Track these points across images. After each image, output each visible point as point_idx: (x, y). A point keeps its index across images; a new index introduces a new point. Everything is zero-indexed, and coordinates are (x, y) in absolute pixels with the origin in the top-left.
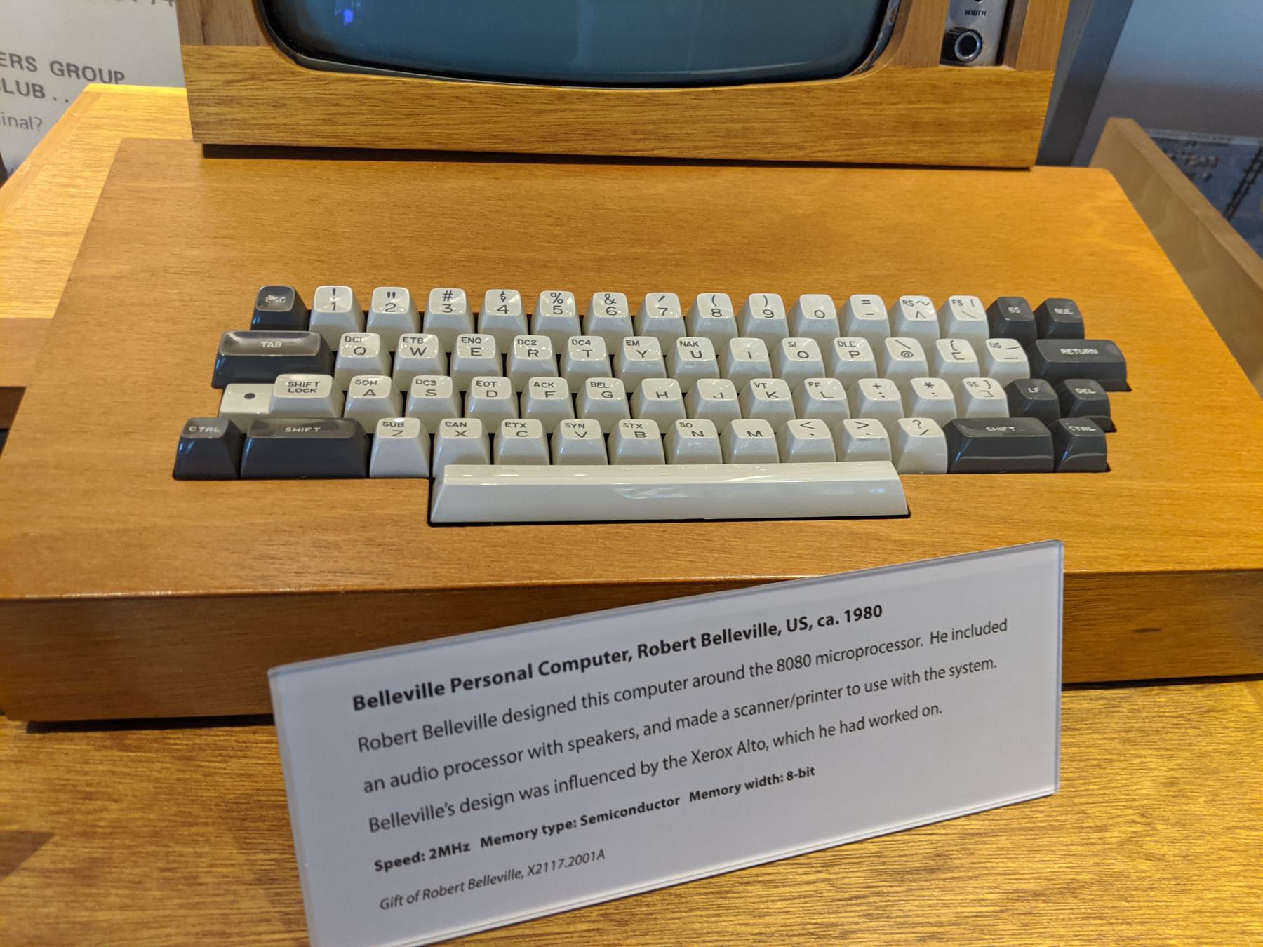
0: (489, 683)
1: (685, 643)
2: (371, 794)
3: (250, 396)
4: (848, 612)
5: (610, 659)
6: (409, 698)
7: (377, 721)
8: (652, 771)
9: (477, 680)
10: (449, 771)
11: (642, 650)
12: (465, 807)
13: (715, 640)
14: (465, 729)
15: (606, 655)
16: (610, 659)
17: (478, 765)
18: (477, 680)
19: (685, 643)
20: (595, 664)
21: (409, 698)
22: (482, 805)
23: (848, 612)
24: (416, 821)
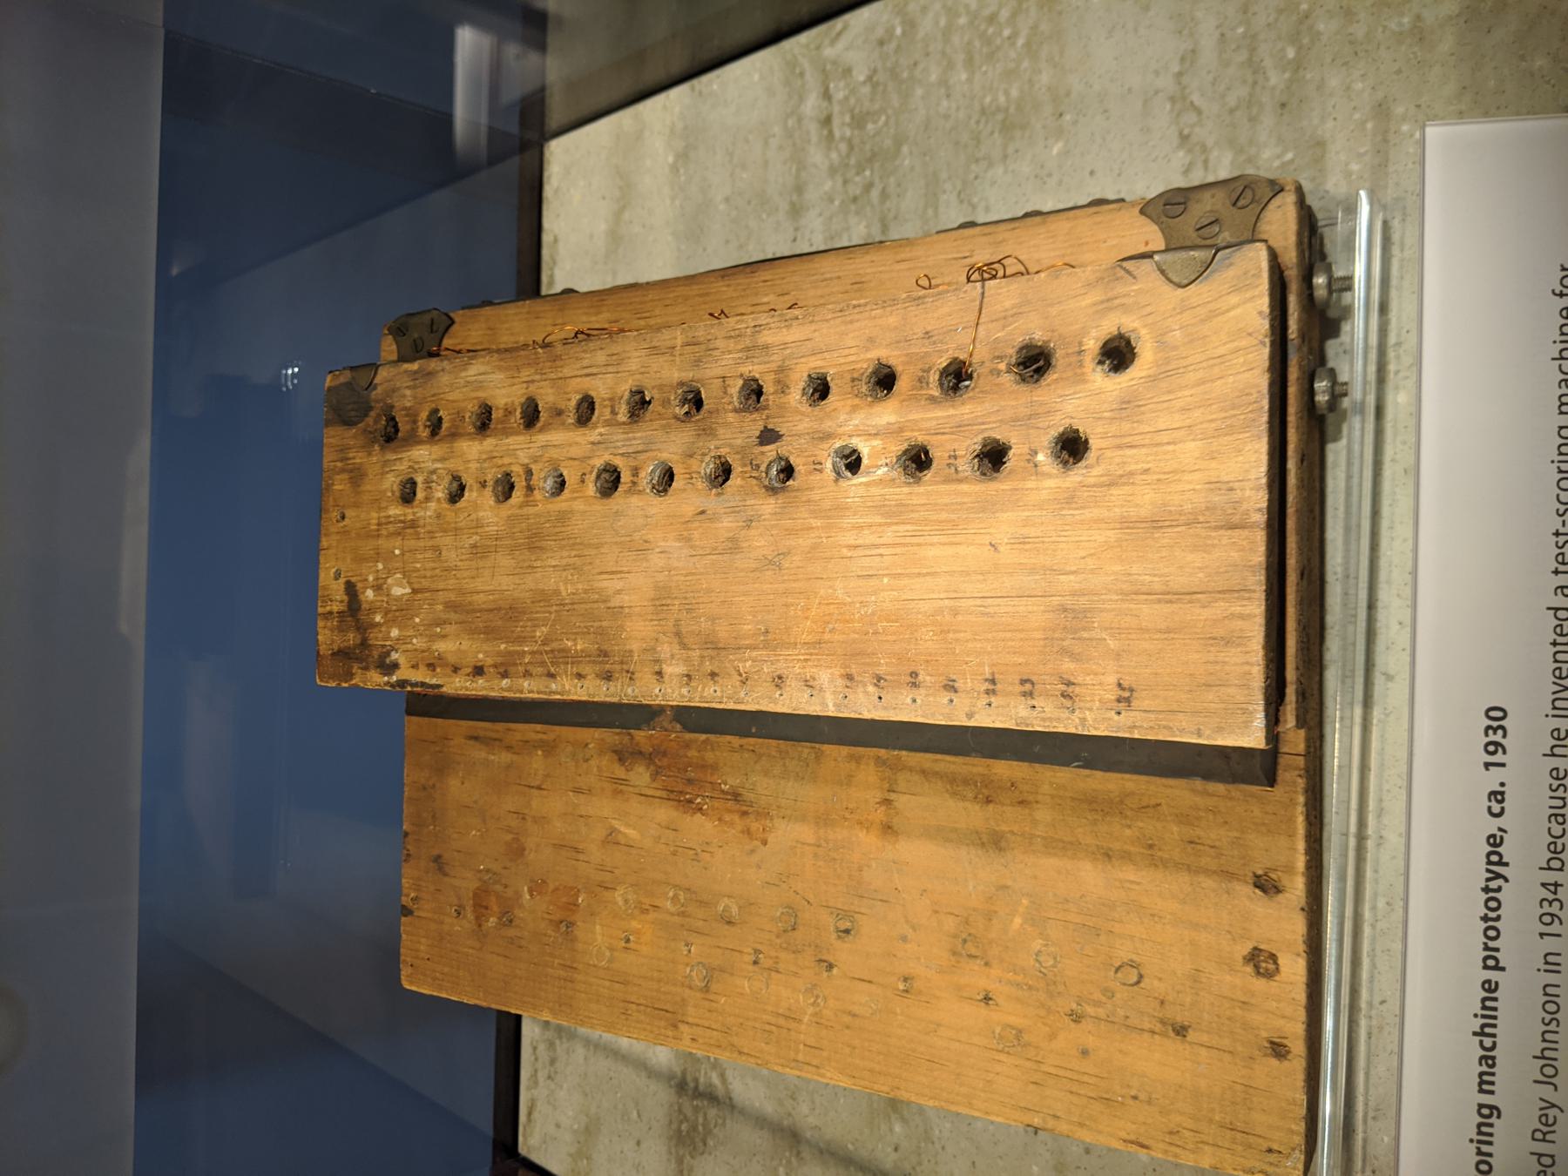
4: (1487, 765)
23: (1487, 765)
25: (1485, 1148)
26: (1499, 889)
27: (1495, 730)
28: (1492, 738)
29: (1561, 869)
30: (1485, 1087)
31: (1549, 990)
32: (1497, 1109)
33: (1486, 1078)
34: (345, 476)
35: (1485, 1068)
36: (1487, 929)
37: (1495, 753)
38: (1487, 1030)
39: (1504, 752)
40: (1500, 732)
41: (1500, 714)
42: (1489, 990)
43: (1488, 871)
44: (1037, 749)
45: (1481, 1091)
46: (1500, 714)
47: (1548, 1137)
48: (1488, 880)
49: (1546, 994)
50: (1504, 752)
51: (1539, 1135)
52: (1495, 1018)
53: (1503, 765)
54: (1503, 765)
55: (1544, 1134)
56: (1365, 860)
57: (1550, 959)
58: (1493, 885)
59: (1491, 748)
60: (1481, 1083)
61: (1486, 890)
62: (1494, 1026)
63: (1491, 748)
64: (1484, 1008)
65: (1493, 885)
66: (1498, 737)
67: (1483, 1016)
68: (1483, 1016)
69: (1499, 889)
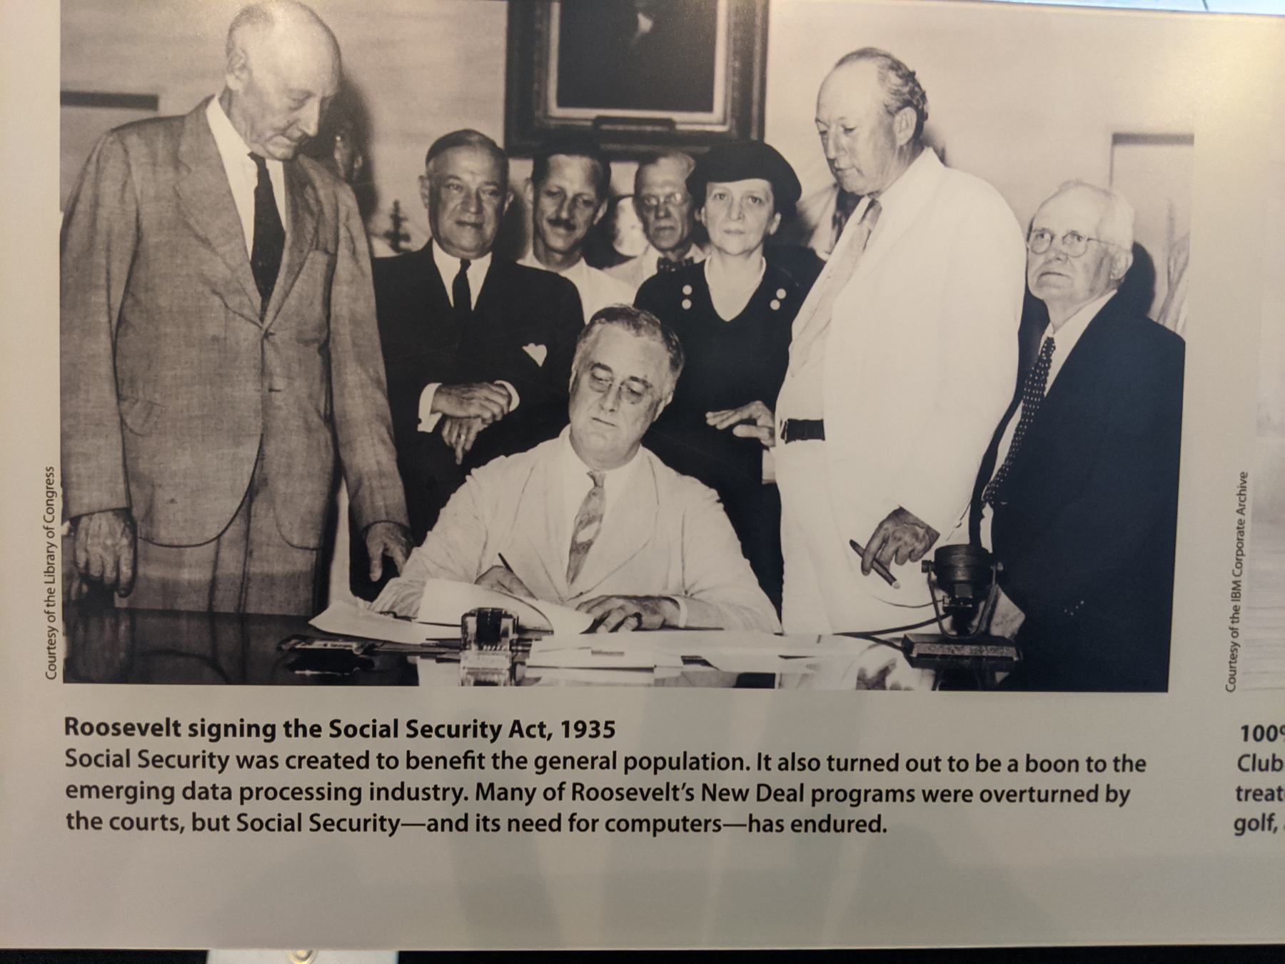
0: (119, 733)
1: (1022, 793)
2: (1270, 803)
3: (466, 799)
4: (566, 724)
5: (688, 825)
6: (143, 733)
7: (82, 776)
8: (1120, 800)
9: (707, 822)
10: (247, 793)
11: (1240, 512)
12: (189, 793)
13: (423, 731)
14: (639, 796)
15: (685, 820)
16: (688, 825)
17: (287, 793)
18: (707, 822)
19: (1022, 793)
20: (257, 727)
21: (143, 733)
22: (305, 795)
23: (566, 724)
24: (645, 798)
26: (484, 736)
27: (595, 729)
28: (589, 727)
29: (759, 799)
31: (1073, 765)
34: (996, 631)
38: (301, 730)
40: (594, 733)
41: (1259, 731)
43: (147, 725)
46: (1259, 731)
47: (578, 796)
48: (492, 727)
49: (1070, 762)
51: (578, 788)
52: (242, 735)
53: (567, 735)
54: (567, 735)
55: (580, 792)
56: (370, 646)
58: (488, 731)
59: (580, 726)
61: (483, 726)
62: (234, 735)
63: (580, 726)
65: (488, 731)
66: (589, 731)
67: (242, 726)
68: (242, 726)
69: (484, 736)
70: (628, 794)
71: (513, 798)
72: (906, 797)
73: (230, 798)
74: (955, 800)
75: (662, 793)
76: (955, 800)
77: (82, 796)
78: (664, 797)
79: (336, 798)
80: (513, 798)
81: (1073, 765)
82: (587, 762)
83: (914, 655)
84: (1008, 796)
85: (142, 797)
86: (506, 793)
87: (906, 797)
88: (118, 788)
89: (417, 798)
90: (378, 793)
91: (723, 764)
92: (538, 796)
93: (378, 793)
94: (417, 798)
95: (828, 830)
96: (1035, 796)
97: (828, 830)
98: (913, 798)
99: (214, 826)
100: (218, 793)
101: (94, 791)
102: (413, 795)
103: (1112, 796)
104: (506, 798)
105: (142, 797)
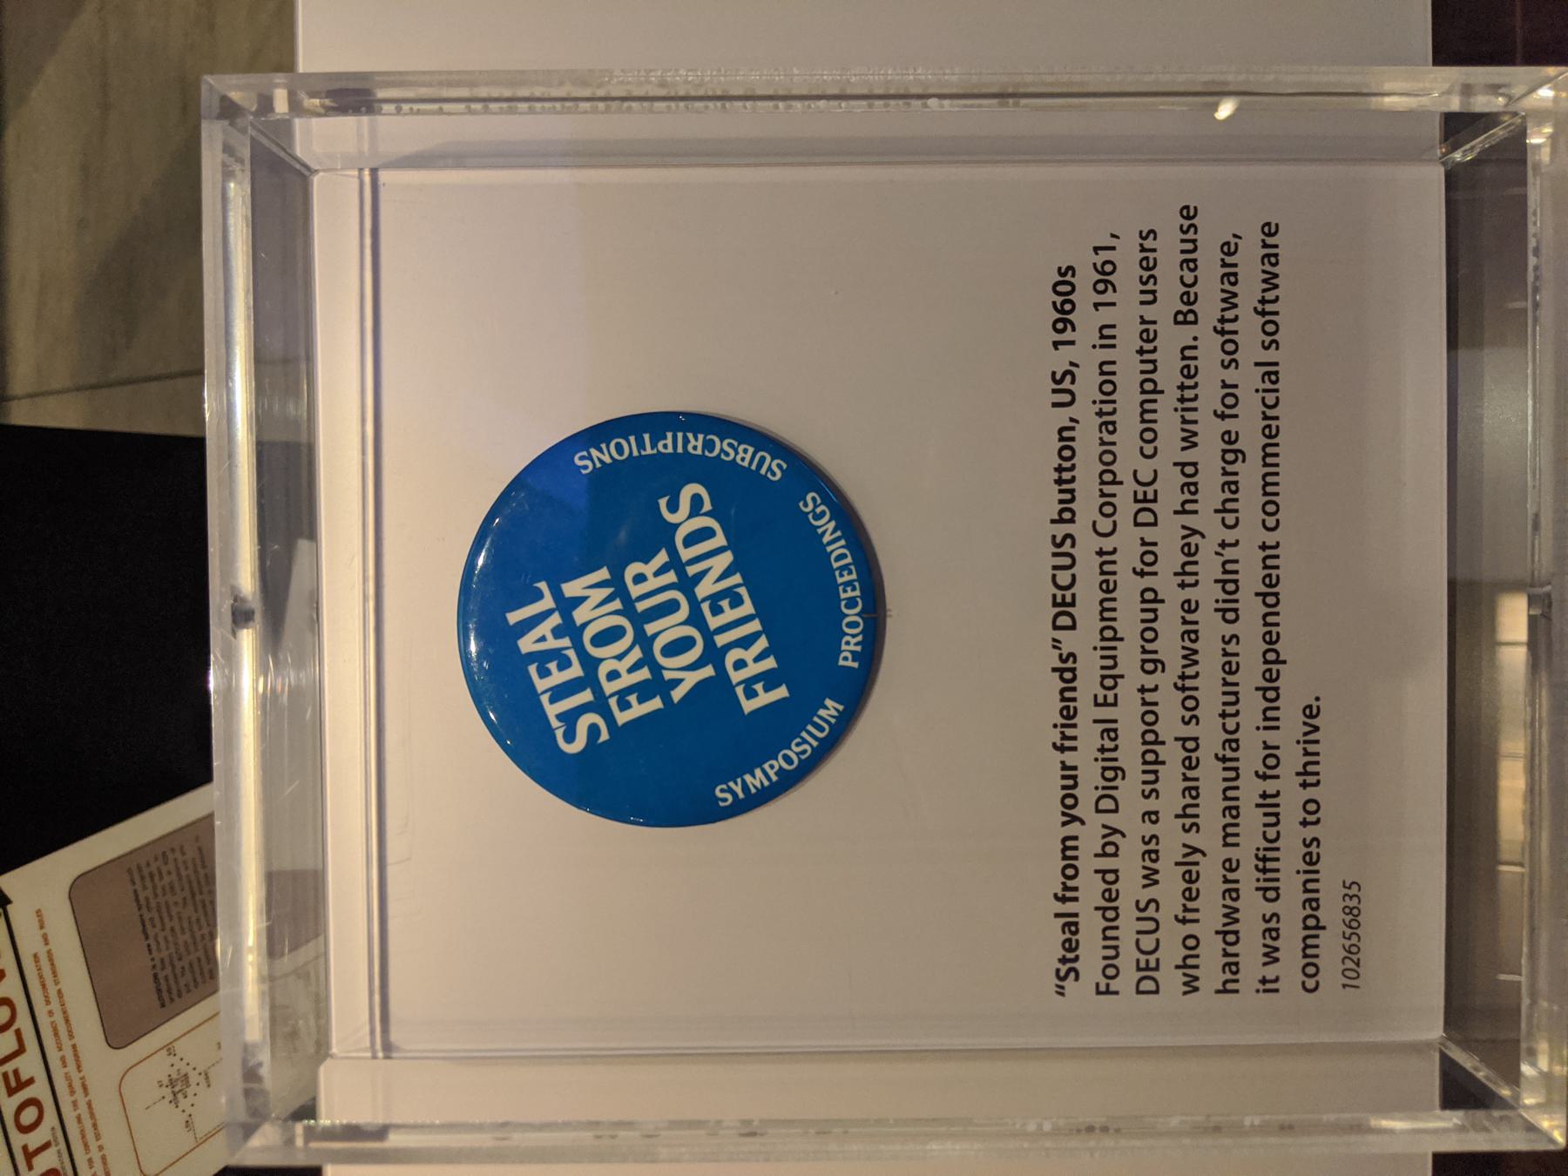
4: (1056, 344)
12: (1230, 616)
22: (1313, 849)
23: (1056, 344)
25: (1311, 748)
30: (1229, 840)
31: (1106, 368)
32: (1243, 453)
33: (1229, 830)
35: (1229, 976)
36: (1065, 867)
37: (1063, 331)
39: (1074, 329)
42: (1189, 554)
43: (1064, 814)
44: (1225, 110)
45: (1226, 845)
49: (1102, 373)
50: (1074, 329)
57: (1106, 332)
60: (1065, 849)
64: (1266, 719)
67: (1306, 872)
68: (1306, 872)
70: (1148, 269)
71: (1317, 891)
72: (1148, 788)
73: (1156, 813)
74: (1277, 418)
75: (1190, 872)
76: (1277, 418)
77: (1074, 700)
78: (1194, 869)
79: (1277, 719)
80: (1317, 891)
81: (1106, 368)
82: (1188, 367)
83: (686, 512)
84: (1311, 716)
85: (1116, 760)
86: (1230, 808)
87: (1148, 788)
88: (1266, 418)
89: (1153, 292)
90: (1270, 721)
91: (1108, 388)
92: (1193, 839)
93: (1270, 721)
94: (1194, 241)
95: (1144, 392)
96: (1230, 710)
97: (1144, 392)
98: (1147, 797)
99: (1150, 367)
100: (1109, 744)
101: (1269, 450)
102: (1190, 246)
103: (1110, 849)
104: (1237, 890)
105: (1116, 760)
